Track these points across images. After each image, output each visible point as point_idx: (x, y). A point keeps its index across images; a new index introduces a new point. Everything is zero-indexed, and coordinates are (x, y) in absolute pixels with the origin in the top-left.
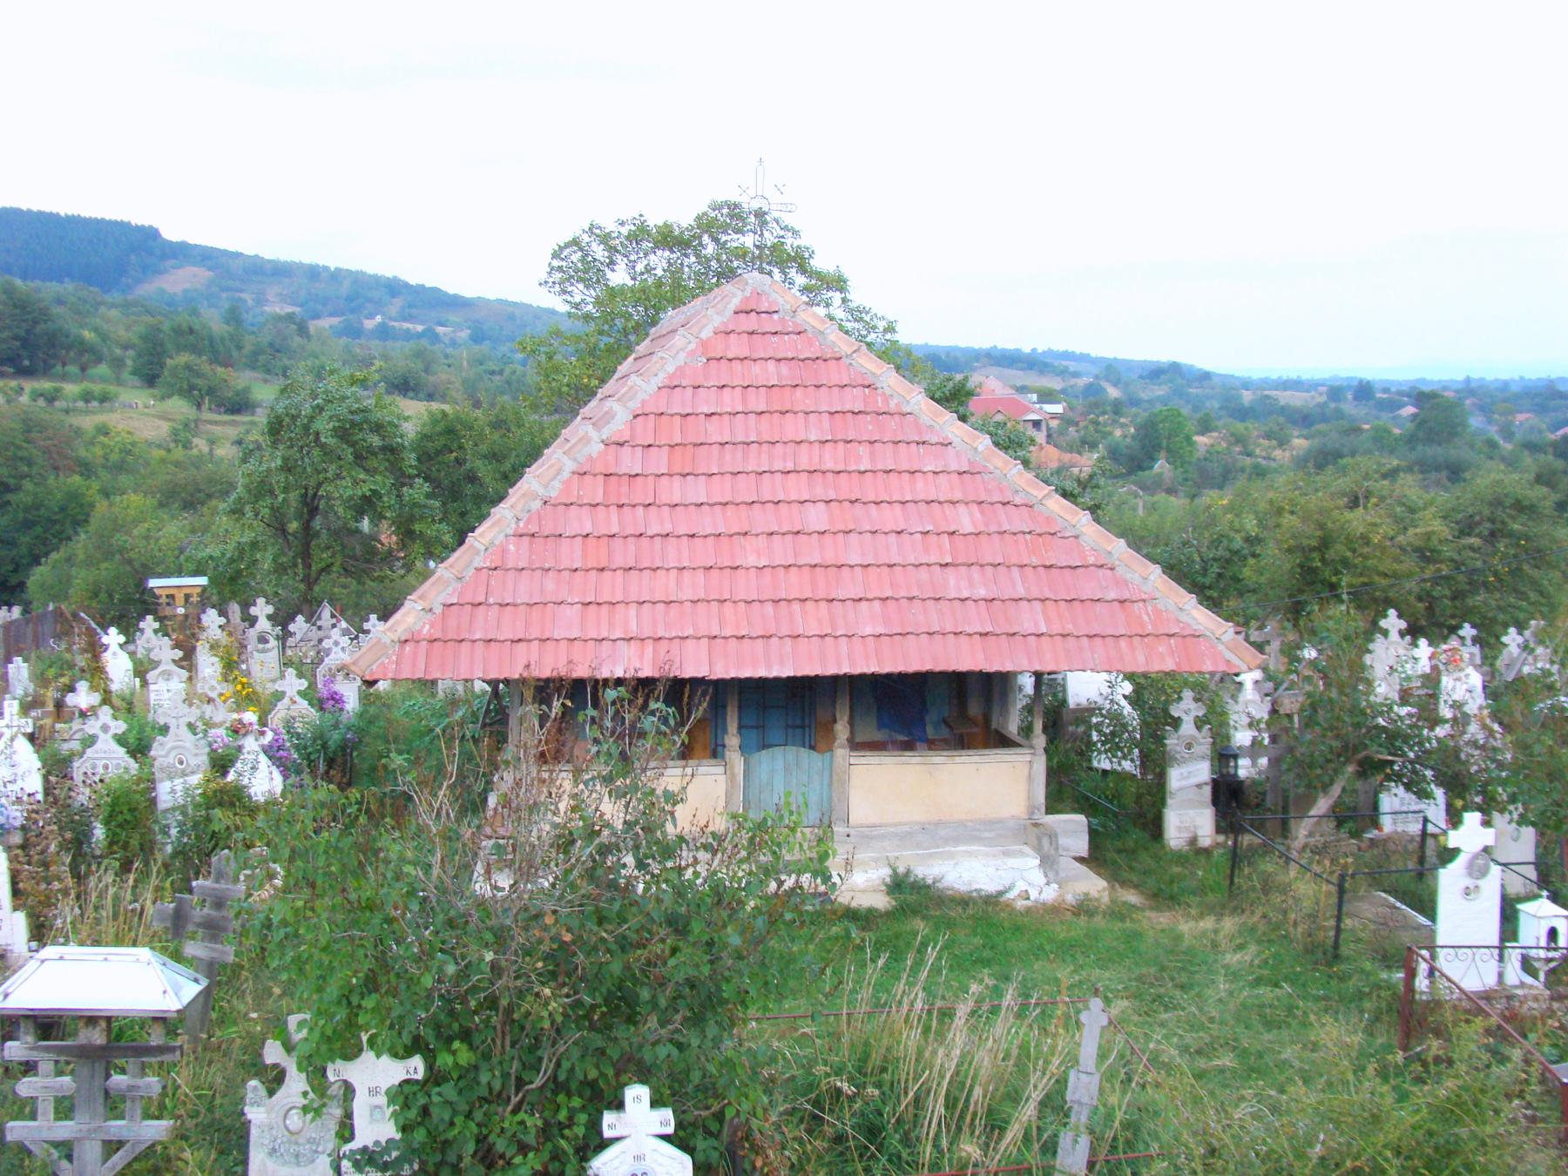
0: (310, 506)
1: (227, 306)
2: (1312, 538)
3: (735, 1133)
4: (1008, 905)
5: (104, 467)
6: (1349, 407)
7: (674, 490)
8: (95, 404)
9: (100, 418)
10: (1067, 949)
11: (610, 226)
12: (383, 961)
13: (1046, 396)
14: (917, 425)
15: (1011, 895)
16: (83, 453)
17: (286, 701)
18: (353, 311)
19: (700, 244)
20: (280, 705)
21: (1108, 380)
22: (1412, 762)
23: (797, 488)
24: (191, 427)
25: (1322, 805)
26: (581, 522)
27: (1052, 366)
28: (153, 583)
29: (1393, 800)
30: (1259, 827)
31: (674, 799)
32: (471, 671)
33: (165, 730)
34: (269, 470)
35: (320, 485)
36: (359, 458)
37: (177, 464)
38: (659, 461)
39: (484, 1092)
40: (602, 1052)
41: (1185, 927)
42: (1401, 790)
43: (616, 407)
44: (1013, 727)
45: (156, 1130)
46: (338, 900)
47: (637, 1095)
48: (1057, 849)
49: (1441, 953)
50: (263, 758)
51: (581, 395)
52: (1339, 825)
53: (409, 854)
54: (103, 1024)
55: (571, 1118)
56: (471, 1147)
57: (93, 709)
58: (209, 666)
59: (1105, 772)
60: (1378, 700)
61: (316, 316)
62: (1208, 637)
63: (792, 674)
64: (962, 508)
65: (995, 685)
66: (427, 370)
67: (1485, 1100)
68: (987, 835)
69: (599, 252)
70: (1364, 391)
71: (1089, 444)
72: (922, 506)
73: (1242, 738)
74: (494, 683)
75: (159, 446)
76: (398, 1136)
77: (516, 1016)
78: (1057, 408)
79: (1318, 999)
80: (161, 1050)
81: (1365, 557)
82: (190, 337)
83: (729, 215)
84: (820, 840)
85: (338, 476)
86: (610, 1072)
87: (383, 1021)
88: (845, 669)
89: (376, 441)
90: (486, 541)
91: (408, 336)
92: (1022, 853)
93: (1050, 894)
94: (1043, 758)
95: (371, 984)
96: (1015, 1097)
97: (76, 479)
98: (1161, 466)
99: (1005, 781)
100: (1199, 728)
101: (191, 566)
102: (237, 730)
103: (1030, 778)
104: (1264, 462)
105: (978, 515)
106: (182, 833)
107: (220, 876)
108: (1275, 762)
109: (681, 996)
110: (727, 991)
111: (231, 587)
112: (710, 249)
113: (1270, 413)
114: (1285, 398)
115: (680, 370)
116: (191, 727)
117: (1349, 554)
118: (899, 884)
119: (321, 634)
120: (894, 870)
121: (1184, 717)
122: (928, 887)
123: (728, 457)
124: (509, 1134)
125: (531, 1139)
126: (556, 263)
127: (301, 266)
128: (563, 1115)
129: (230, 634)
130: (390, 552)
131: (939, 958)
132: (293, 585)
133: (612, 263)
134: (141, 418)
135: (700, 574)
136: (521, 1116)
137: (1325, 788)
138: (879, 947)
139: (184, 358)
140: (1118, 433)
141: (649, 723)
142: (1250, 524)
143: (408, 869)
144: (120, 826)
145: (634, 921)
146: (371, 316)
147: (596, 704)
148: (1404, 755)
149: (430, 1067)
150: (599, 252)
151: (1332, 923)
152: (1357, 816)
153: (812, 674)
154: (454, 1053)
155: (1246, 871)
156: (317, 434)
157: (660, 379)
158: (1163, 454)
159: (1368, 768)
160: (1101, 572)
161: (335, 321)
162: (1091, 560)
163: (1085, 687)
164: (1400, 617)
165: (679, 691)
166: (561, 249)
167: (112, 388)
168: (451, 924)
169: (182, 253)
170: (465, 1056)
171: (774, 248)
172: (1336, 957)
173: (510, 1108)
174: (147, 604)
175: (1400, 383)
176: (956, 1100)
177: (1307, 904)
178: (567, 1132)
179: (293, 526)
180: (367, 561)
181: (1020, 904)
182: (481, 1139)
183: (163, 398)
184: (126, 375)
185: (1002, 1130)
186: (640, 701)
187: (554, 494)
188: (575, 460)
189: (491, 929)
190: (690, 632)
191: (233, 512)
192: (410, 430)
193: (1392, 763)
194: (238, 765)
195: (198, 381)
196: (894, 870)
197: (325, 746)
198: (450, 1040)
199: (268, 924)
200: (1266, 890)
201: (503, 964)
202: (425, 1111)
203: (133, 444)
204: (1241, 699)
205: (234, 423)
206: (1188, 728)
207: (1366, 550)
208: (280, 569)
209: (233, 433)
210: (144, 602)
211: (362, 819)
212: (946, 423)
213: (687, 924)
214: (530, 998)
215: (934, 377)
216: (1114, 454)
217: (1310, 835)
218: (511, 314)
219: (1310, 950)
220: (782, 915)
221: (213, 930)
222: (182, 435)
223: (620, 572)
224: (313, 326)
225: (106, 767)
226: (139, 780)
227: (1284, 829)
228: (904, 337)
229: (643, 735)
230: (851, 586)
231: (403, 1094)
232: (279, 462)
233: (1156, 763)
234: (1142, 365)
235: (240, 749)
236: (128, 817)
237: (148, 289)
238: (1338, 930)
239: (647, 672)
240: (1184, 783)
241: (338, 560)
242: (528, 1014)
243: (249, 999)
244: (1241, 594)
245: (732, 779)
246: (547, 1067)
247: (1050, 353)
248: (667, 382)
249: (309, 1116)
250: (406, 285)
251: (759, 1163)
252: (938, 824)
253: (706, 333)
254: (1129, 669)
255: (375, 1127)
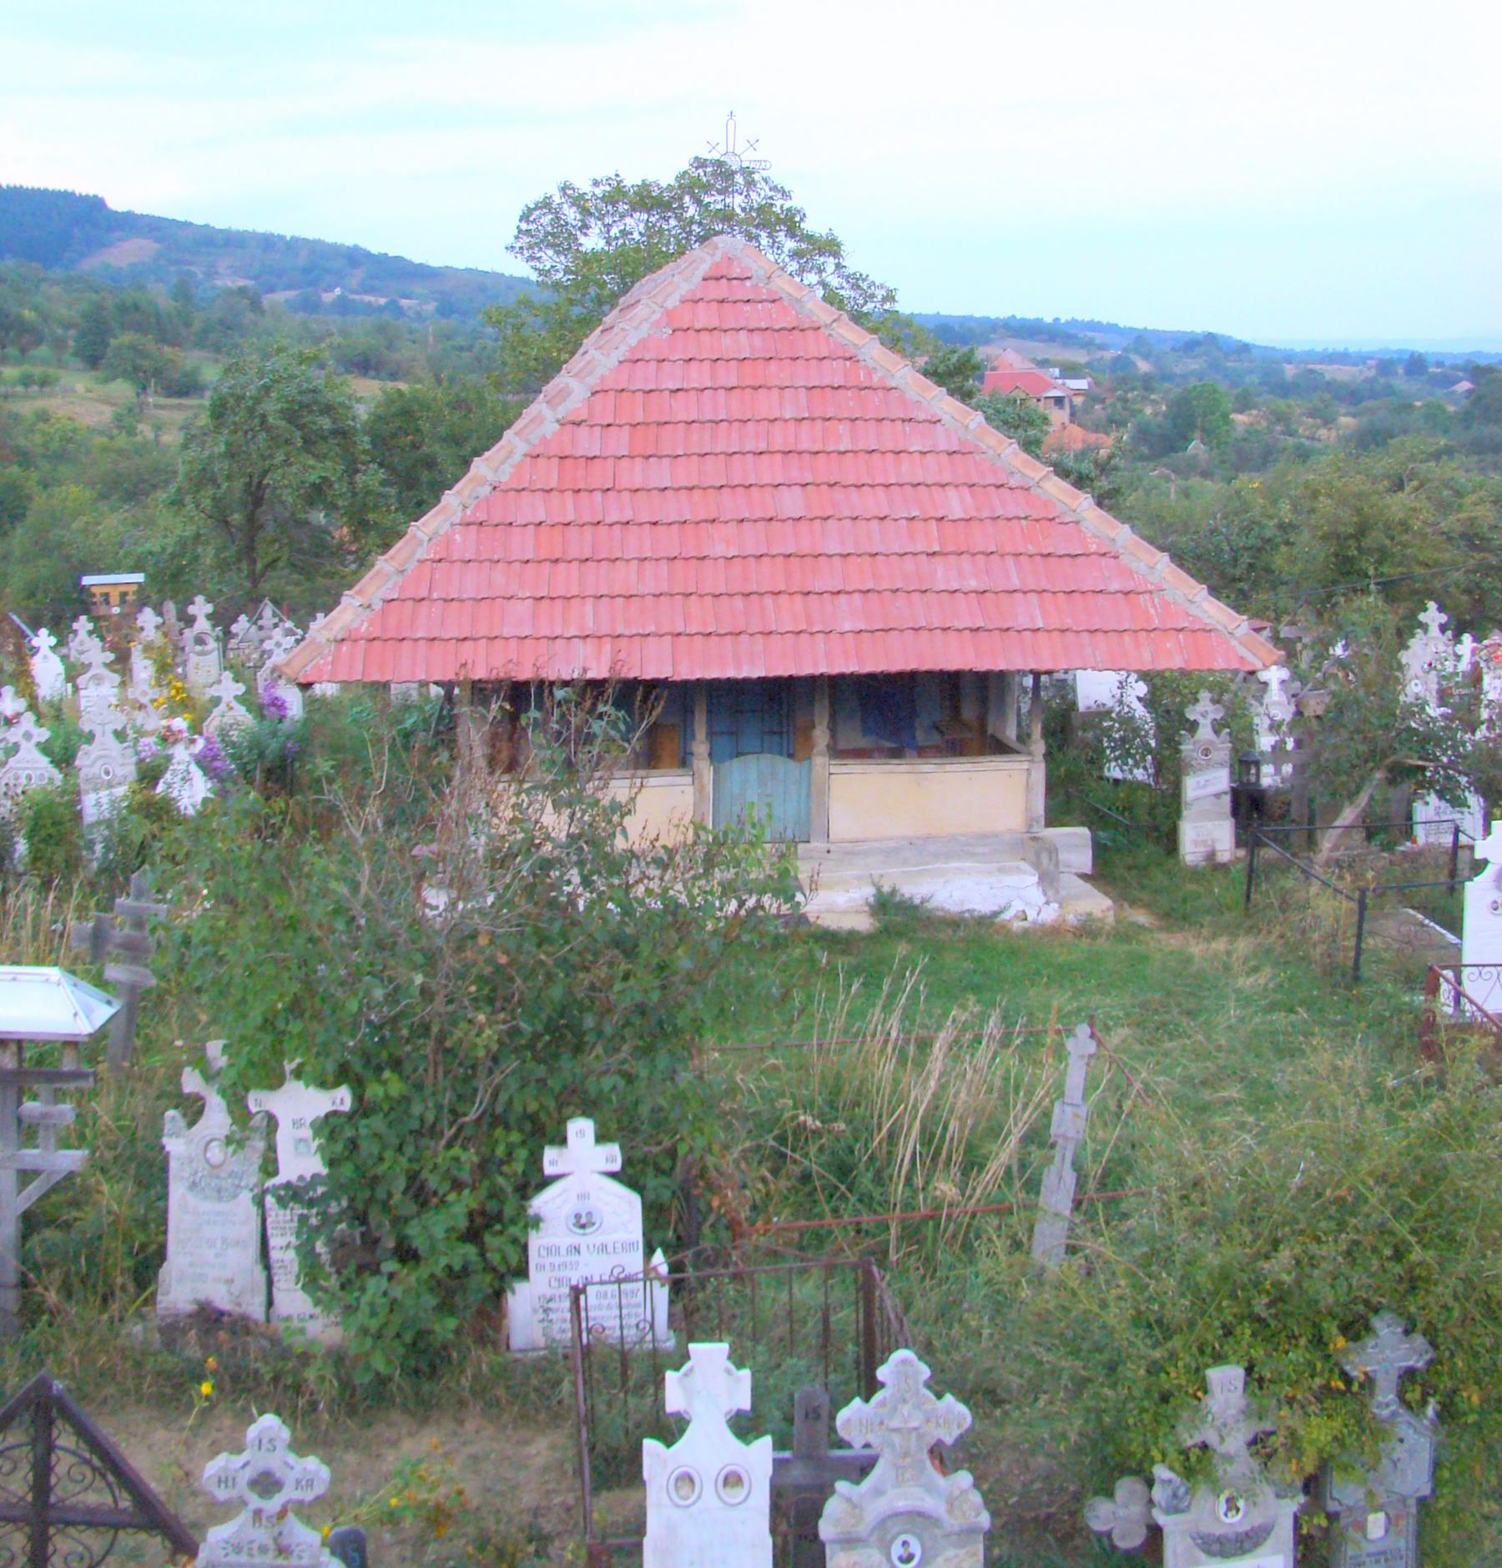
0: (256, 496)
1: (175, 280)
2: (1348, 521)
3: (688, 1172)
4: (1004, 928)
5: (44, 456)
6: (1400, 383)
7: (634, 474)
8: (35, 388)
9: (40, 404)
10: (1064, 974)
11: (585, 187)
12: (309, 985)
13: (1070, 371)
14: (903, 401)
15: (1006, 916)
16: (22, 442)
17: (222, 707)
18: (311, 284)
19: (681, 207)
20: (216, 712)
21: (1136, 352)
22: (1445, 768)
23: (770, 470)
24: (136, 411)
25: (1348, 815)
26: (534, 509)
27: (1075, 337)
28: (87, 580)
29: (1428, 808)
30: (1282, 840)
31: (625, 810)
32: (416, 673)
33: (90, 738)
34: (211, 457)
35: (266, 472)
36: (308, 442)
37: (120, 452)
38: (620, 442)
39: (416, 1125)
40: (542, 1082)
41: (1196, 949)
42: (1432, 798)
43: (574, 384)
44: (1011, 733)
45: (71, 1159)
46: (262, 919)
47: (581, 1129)
48: (1057, 865)
49: (1466, 972)
50: (194, 768)
51: (550, 368)
52: (1369, 836)
53: (333, 868)
54: (14, 1048)
55: (510, 1154)
56: (401, 1183)
57: (18, 715)
58: (143, 668)
59: (1116, 781)
60: (1409, 700)
61: (271, 290)
62: (1227, 634)
63: (763, 674)
64: (951, 492)
65: (987, 687)
66: (389, 347)
67: (1475, 1124)
68: (980, 850)
69: (571, 214)
70: (1416, 364)
71: (1114, 422)
72: (908, 489)
73: (1265, 742)
74: (448, 686)
75: (101, 433)
76: (325, 1171)
77: (448, 1044)
78: (1082, 384)
79: (1335, 1025)
80: (76, 1075)
81: (1405, 546)
82: (134, 315)
83: (713, 174)
84: (782, 856)
85: (287, 462)
86: (551, 1104)
87: (308, 1049)
88: (823, 668)
89: (326, 423)
90: (430, 529)
91: (370, 309)
92: (1018, 870)
93: (1050, 914)
94: (1043, 765)
95: (295, 1008)
96: (996, 1132)
97: (15, 470)
98: (1196, 447)
99: (998, 792)
100: (1217, 732)
101: (130, 562)
102: (168, 738)
103: (1028, 788)
104: (1307, 443)
105: (968, 499)
106: (107, 849)
107: (139, 895)
108: (1299, 769)
109: (627, 1024)
110: (681, 1020)
111: (170, 582)
112: (692, 211)
113: (1315, 389)
114: (1331, 372)
115: (642, 343)
116: (120, 735)
117: (1387, 542)
118: (885, 905)
119: (262, 634)
120: (879, 889)
121: (1201, 721)
122: (916, 907)
123: (695, 438)
124: (443, 1169)
125: (465, 1175)
126: (524, 226)
127: (254, 235)
128: (500, 1151)
129: (166, 635)
130: (341, 545)
131: (915, 989)
132: (238, 578)
133: (585, 227)
134: (83, 402)
135: (664, 565)
136: (456, 1150)
137: (1352, 796)
138: (852, 972)
139: (127, 338)
140: (1148, 411)
141: (597, 727)
142: (1285, 509)
143: (333, 885)
144: (44, 840)
145: (578, 941)
146: (329, 289)
147: (540, 706)
148: (1437, 759)
149: (359, 1098)
150: (571, 214)
151: (1352, 942)
152: (1386, 828)
153: (786, 674)
154: (385, 1083)
155: (1264, 886)
156: (264, 416)
157: (621, 353)
158: (1197, 434)
159: (1399, 773)
160: (1103, 561)
161: (291, 294)
162: (1093, 548)
163: (1095, 688)
164: (1441, 609)
165: (633, 694)
166: (530, 211)
167: (52, 371)
168: (380, 946)
169: (130, 223)
170: (395, 1085)
171: (760, 209)
172: (1357, 979)
173: (443, 1142)
174: (83, 603)
175: (1454, 356)
176: (932, 1135)
177: (1327, 924)
178: (505, 1168)
179: (237, 518)
180: (317, 555)
181: (1017, 925)
182: (413, 1177)
183: (107, 381)
184: (67, 357)
185: (982, 1167)
186: (588, 704)
187: (504, 478)
188: (527, 441)
189: (421, 950)
190: (652, 629)
191: (173, 503)
192: (363, 412)
193: (1423, 769)
194: (168, 776)
195: (145, 363)
196: (879, 889)
197: (261, 755)
198: (379, 1069)
199: (186, 941)
200: (1284, 906)
201: (434, 987)
202: (353, 1145)
203: (74, 431)
204: (1266, 700)
205: (180, 407)
206: (1205, 732)
207: (1405, 537)
208: (223, 566)
209: (180, 417)
210: (83, 602)
211: (287, 831)
212: (940, 402)
213: (636, 946)
214: (463, 1025)
215: (937, 349)
216: (1143, 434)
217: (1336, 847)
218: (481, 284)
219: (1328, 972)
220: (738, 937)
221: (134, 951)
222: (126, 421)
223: (575, 564)
224: (267, 300)
225: (29, 778)
226: (64, 792)
227: (1311, 842)
228: (905, 306)
229: (590, 738)
230: (827, 578)
231: (329, 1126)
232: (223, 448)
233: (1170, 767)
234: (1175, 336)
235: (169, 758)
236: (52, 831)
237: (92, 264)
238: (1359, 951)
239: (597, 672)
240: (1201, 792)
241: (286, 552)
242: (461, 1041)
243: (175, 1027)
244: (1274, 588)
245: (700, 791)
246: (483, 1098)
247: (1073, 323)
248: (628, 356)
249: (231, 1149)
250: (368, 255)
251: (715, 1203)
252: (928, 838)
253: (673, 302)
254: (1146, 668)
255: (301, 1161)
